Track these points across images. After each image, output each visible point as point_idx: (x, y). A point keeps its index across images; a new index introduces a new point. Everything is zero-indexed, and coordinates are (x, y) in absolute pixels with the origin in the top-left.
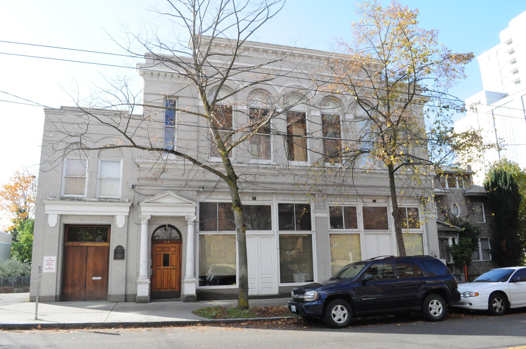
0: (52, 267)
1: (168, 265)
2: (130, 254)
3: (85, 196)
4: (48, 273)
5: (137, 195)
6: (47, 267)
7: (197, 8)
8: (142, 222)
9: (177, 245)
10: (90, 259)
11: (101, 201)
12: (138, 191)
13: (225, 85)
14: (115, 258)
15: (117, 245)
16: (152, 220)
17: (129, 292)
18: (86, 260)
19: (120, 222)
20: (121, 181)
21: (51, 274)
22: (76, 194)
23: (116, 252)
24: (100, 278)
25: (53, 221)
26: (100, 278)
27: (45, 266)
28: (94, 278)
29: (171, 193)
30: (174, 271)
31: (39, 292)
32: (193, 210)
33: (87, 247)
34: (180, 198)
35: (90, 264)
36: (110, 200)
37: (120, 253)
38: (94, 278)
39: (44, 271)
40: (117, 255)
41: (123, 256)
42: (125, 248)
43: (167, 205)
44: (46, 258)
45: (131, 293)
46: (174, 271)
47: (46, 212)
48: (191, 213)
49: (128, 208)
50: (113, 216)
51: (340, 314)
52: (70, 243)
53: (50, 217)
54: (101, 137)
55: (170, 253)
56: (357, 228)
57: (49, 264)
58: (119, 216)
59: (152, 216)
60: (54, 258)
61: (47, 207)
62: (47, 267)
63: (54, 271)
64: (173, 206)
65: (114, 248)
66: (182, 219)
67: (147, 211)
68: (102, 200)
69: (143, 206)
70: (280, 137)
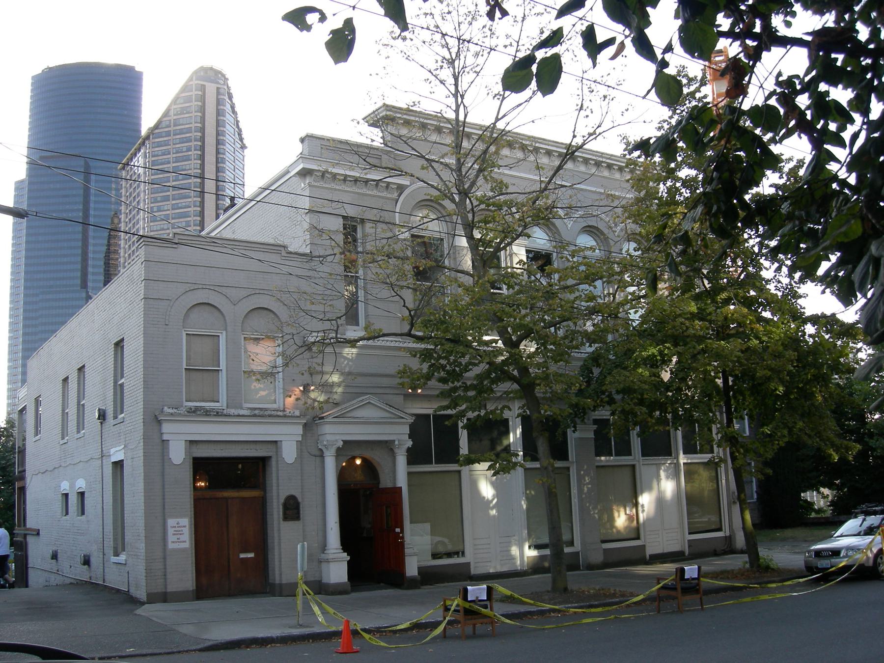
0: (182, 538)
2: (308, 511)
4: (174, 550)
6: (175, 538)
11: (255, 416)
14: (286, 518)
15: (288, 494)
16: (348, 448)
19: (289, 453)
21: (184, 550)
22: (203, 401)
24: (251, 555)
25: (178, 454)
26: (251, 555)
27: (171, 538)
28: (242, 556)
31: (281, 580)
32: (407, 430)
33: (226, 499)
36: (269, 412)
38: (242, 556)
39: (171, 546)
40: (288, 512)
41: (298, 513)
42: (300, 500)
45: (312, 579)
47: (165, 437)
48: (400, 435)
50: (276, 442)
54: (244, 293)
56: (630, 454)
57: (178, 533)
58: (289, 441)
59: (345, 442)
62: (175, 538)
63: (187, 545)
64: (376, 423)
66: (388, 446)
67: (334, 434)
68: (257, 412)
70: (408, 327)
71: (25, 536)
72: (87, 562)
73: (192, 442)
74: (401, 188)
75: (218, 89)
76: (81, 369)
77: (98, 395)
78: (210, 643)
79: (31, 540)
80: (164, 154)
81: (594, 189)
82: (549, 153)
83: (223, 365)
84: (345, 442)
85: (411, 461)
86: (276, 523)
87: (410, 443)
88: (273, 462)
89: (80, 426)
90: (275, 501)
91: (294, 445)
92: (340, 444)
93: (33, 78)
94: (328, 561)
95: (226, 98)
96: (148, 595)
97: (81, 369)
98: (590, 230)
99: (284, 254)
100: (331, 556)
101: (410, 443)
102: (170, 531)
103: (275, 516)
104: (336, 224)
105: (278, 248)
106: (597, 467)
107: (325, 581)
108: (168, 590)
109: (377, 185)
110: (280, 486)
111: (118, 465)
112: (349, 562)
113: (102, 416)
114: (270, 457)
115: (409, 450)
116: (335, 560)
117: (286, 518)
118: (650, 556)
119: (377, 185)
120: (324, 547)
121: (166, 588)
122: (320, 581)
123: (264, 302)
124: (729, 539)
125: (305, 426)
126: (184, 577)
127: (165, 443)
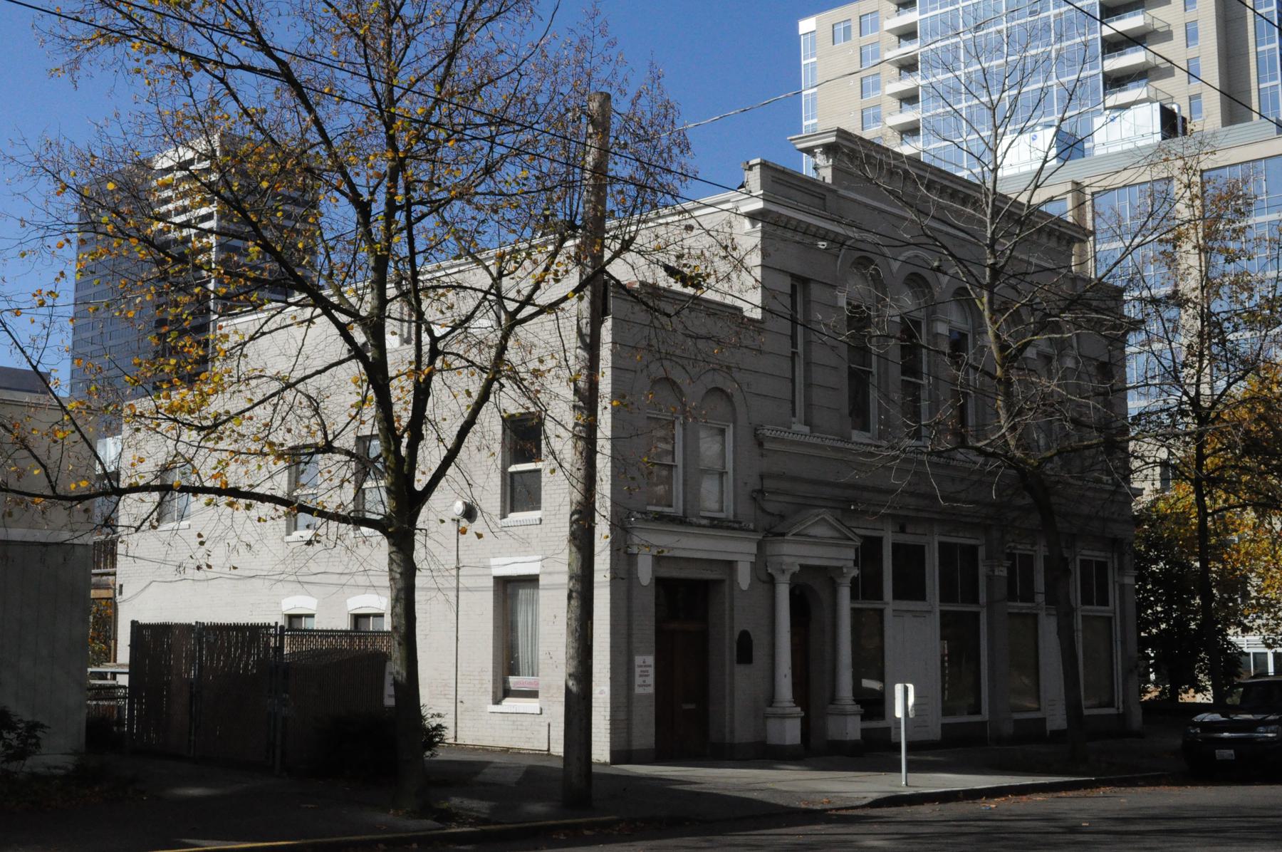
2: (759, 652)
4: (641, 695)
19: (744, 578)
24: (692, 706)
25: (645, 572)
26: (692, 706)
32: (851, 554)
81: (875, 204)
84: (804, 568)
85: (854, 597)
91: (748, 566)
92: (797, 568)
101: (855, 572)
106: (1010, 614)
108: (634, 748)
111: (510, 589)
115: (854, 581)
120: (772, 699)
121: (629, 741)
123: (730, 387)
124: (1122, 718)
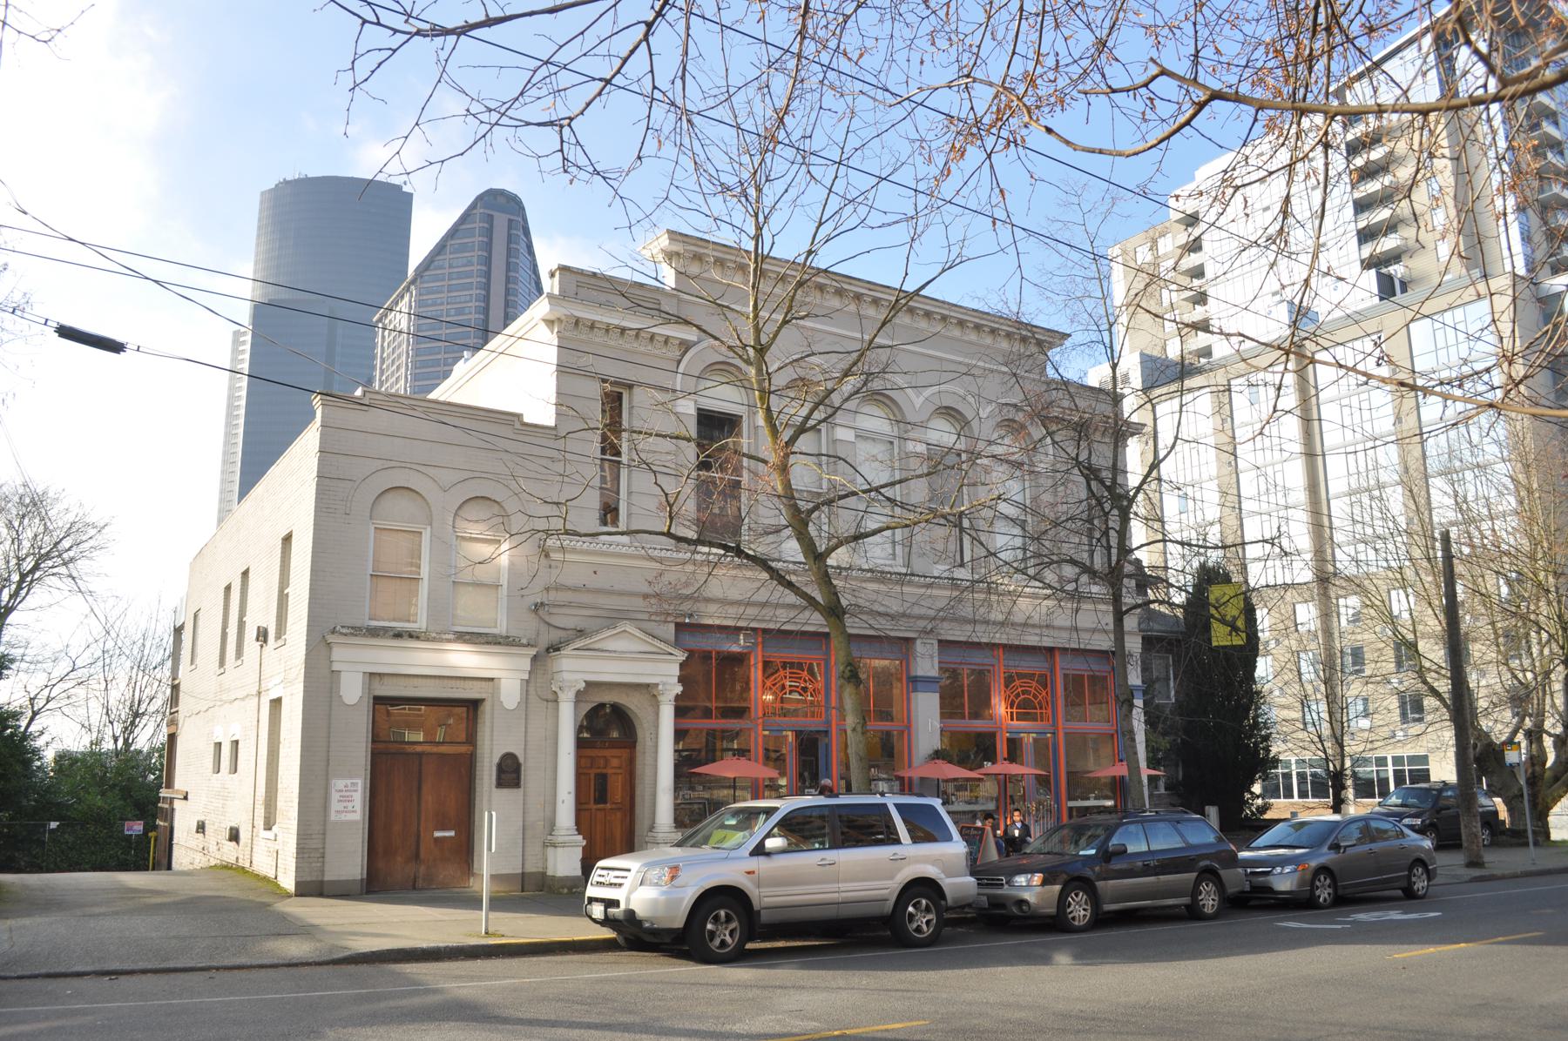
1: (605, 802)
3: (421, 624)
5: (544, 628)
6: (340, 807)
7: (761, 219)
8: (562, 696)
9: (625, 753)
10: (426, 788)
12: (547, 618)
13: (468, 287)
14: (501, 784)
17: (530, 868)
18: (419, 788)
20: (504, 591)
21: (356, 822)
23: (501, 769)
24: (452, 833)
25: (352, 691)
26: (452, 833)
27: (335, 806)
28: (438, 834)
29: (630, 628)
30: (619, 814)
34: (650, 639)
35: (429, 799)
37: (510, 772)
38: (438, 834)
39: (333, 817)
42: (521, 760)
43: (620, 656)
44: (339, 784)
46: (619, 814)
47: (336, 667)
48: (666, 674)
49: (528, 661)
51: (725, 934)
52: (463, 749)
53: (344, 677)
55: (610, 771)
60: (360, 782)
61: (338, 654)
65: (496, 760)
66: (648, 690)
67: (574, 670)
69: (568, 656)
71: (172, 800)
72: (234, 836)
73: (371, 674)
74: (686, 346)
75: (510, 221)
76: (245, 574)
77: (261, 612)
78: (347, 953)
79: (177, 804)
80: (434, 304)
82: (876, 302)
83: (425, 572)
86: (486, 788)
87: (679, 689)
88: (486, 708)
89: (239, 653)
90: (486, 760)
93: (263, 194)
94: (554, 846)
95: (521, 233)
96: (298, 884)
97: (245, 574)
98: (949, 412)
99: (518, 426)
100: (560, 839)
101: (679, 689)
102: (335, 796)
103: (486, 778)
104: (594, 390)
105: (512, 419)
107: (550, 873)
109: (637, 336)
110: (493, 745)
112: (584, 848)
113: (262, 635)
114: (483, 700)
116: (564, 845)
117: (501, 784)
118: (61, 757)
119: (637, 336)
121: (323, 872)
122: (544, 874)
125: (535, 659)
126: (350, 863)
127: (335, 674)
